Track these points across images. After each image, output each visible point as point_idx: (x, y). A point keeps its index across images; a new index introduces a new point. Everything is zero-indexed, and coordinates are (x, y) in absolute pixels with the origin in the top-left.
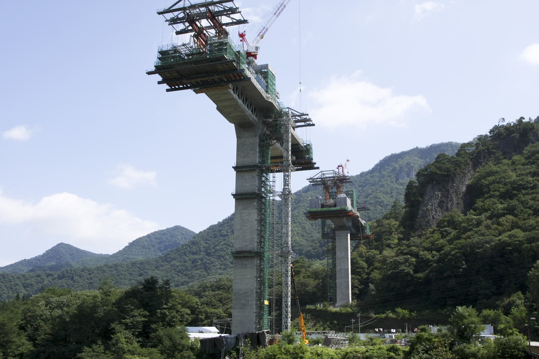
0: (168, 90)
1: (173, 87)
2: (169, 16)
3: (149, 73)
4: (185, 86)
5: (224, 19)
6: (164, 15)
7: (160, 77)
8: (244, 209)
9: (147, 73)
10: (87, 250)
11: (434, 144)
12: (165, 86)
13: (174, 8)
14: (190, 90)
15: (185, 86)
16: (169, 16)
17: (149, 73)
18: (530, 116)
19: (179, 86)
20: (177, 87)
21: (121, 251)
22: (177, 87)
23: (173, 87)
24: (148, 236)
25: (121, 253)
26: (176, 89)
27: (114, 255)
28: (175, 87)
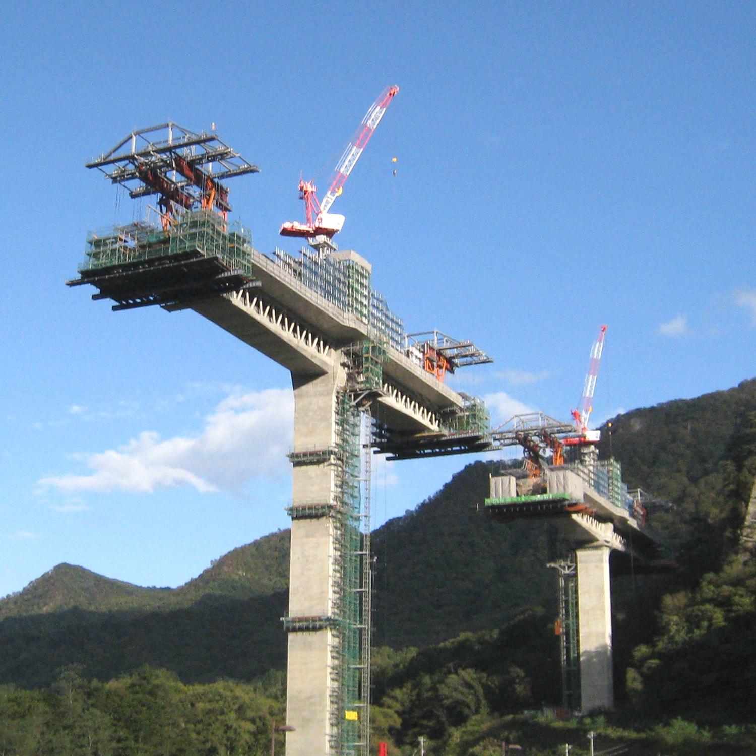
0: (115, 309)
1: (131, 302)
2: (113, 170)
3: (72, 284)
4: (144, 299)
5: (210, 168)
6: (100, 167)
7: (93, 287)
8: (307, 536)
9: (68, 284)
10: (710, 391)
11: (745, 380)
12: (110, 303)
13: (112, 158)
14: (157, 307)
15: (144, 299)
16: (113, 170)
17: (72, 284)
18: (749, 377)
19: (134, 301)
20: (138, 301)
21: (196, 579)
22: (138, 301)
23: (131, 302)
24: (256, 544)
25: (195, 585)
26: (129, 306)
27: (182, 590)
28: (127, 302)
